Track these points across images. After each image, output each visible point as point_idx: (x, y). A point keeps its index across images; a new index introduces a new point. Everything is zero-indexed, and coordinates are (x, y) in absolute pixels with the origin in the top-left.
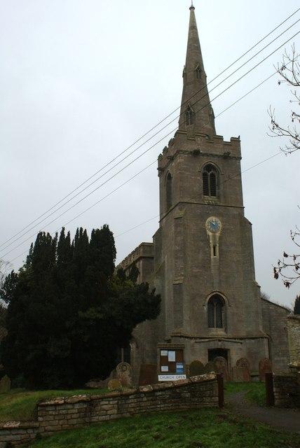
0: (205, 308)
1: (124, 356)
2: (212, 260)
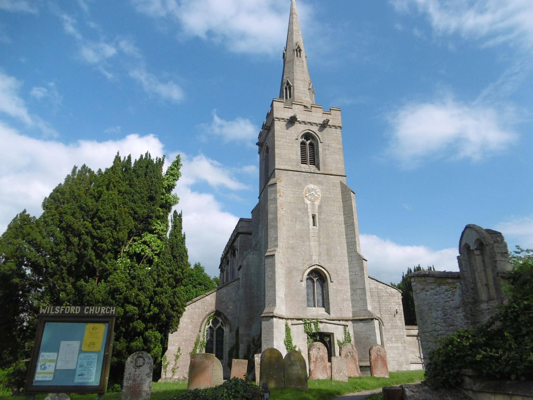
0: (304, 284)
1: (217, 341)
2: (311, 231)
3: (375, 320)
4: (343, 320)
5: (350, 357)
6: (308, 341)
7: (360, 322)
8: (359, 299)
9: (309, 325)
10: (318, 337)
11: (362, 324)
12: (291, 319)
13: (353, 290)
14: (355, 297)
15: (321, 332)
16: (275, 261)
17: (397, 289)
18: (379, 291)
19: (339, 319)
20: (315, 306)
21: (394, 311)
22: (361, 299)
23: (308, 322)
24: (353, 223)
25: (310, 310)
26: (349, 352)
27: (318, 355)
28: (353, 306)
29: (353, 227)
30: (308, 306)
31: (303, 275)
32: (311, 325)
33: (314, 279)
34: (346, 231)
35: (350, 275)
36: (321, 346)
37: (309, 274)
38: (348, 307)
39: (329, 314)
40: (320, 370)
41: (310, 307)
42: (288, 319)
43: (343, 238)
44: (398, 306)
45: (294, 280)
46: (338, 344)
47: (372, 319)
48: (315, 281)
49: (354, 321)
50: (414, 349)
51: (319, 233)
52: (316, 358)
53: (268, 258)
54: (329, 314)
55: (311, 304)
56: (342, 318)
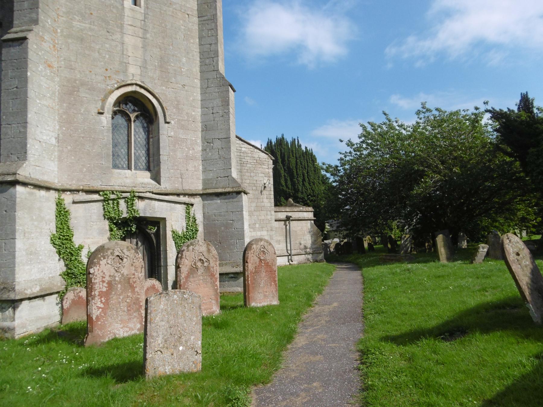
0: (106, 120)
2: (127, 12)
3: (243, 194)
4: (185, 195)
5: (201, 271)
6: (111, 234)
7: (216, 198)
8: (217, 157)
9: (113, 203)
10: (134, 226)
11: (219, 201)
12: (70, 191)
13: (207, 142)
14: (210, 154)
15: (141, 217)
16: (26, 53)
17: (267, 154)
18: (242, 154)
19: (178, 192)
20: (129, 168)
21: (261, 185)
22: (220, 158)
23: (113, 196)
24: (215, 16)
25: (120, 174)
26: (200, 260)
27: (117, 274)
28: (205, 171)
29: (213, 25)
30: (115, 166)
31: (104, 100)
32: (118, 203)
33: (131, 115)
34: (201, 30)
35: (203, 114)
36: (125, 251)
37: (119, 102)
38: (195, 171)
39: (159, 183)
40: (121, 313)
41: (118, 168)
42: (64, 191)
43: (193, 43)
44: (266, 178)
45: (82, 110)
46: (173, 237)
47: (239, 193)
48: (133, 119)
49: (205, 196)
50: (279, 238)
51: (144, 21)
52: (109, 283)
53: (10, 46)
54: (159, 183)
55: (122, 163)
56: (184, 190)
